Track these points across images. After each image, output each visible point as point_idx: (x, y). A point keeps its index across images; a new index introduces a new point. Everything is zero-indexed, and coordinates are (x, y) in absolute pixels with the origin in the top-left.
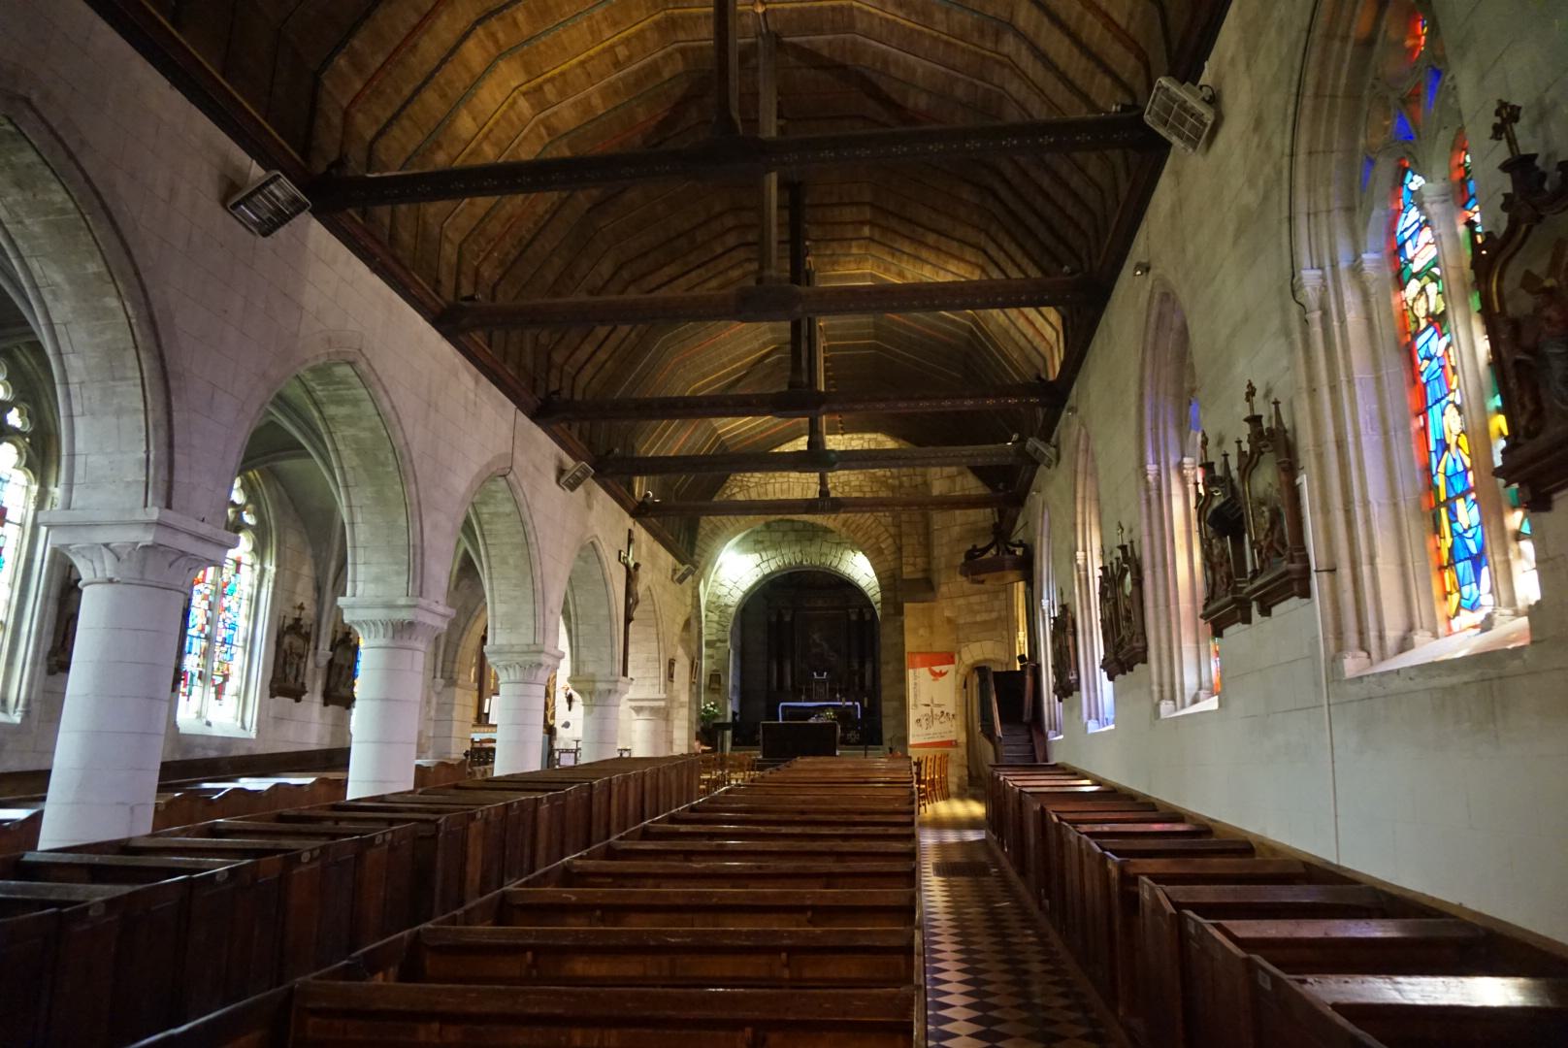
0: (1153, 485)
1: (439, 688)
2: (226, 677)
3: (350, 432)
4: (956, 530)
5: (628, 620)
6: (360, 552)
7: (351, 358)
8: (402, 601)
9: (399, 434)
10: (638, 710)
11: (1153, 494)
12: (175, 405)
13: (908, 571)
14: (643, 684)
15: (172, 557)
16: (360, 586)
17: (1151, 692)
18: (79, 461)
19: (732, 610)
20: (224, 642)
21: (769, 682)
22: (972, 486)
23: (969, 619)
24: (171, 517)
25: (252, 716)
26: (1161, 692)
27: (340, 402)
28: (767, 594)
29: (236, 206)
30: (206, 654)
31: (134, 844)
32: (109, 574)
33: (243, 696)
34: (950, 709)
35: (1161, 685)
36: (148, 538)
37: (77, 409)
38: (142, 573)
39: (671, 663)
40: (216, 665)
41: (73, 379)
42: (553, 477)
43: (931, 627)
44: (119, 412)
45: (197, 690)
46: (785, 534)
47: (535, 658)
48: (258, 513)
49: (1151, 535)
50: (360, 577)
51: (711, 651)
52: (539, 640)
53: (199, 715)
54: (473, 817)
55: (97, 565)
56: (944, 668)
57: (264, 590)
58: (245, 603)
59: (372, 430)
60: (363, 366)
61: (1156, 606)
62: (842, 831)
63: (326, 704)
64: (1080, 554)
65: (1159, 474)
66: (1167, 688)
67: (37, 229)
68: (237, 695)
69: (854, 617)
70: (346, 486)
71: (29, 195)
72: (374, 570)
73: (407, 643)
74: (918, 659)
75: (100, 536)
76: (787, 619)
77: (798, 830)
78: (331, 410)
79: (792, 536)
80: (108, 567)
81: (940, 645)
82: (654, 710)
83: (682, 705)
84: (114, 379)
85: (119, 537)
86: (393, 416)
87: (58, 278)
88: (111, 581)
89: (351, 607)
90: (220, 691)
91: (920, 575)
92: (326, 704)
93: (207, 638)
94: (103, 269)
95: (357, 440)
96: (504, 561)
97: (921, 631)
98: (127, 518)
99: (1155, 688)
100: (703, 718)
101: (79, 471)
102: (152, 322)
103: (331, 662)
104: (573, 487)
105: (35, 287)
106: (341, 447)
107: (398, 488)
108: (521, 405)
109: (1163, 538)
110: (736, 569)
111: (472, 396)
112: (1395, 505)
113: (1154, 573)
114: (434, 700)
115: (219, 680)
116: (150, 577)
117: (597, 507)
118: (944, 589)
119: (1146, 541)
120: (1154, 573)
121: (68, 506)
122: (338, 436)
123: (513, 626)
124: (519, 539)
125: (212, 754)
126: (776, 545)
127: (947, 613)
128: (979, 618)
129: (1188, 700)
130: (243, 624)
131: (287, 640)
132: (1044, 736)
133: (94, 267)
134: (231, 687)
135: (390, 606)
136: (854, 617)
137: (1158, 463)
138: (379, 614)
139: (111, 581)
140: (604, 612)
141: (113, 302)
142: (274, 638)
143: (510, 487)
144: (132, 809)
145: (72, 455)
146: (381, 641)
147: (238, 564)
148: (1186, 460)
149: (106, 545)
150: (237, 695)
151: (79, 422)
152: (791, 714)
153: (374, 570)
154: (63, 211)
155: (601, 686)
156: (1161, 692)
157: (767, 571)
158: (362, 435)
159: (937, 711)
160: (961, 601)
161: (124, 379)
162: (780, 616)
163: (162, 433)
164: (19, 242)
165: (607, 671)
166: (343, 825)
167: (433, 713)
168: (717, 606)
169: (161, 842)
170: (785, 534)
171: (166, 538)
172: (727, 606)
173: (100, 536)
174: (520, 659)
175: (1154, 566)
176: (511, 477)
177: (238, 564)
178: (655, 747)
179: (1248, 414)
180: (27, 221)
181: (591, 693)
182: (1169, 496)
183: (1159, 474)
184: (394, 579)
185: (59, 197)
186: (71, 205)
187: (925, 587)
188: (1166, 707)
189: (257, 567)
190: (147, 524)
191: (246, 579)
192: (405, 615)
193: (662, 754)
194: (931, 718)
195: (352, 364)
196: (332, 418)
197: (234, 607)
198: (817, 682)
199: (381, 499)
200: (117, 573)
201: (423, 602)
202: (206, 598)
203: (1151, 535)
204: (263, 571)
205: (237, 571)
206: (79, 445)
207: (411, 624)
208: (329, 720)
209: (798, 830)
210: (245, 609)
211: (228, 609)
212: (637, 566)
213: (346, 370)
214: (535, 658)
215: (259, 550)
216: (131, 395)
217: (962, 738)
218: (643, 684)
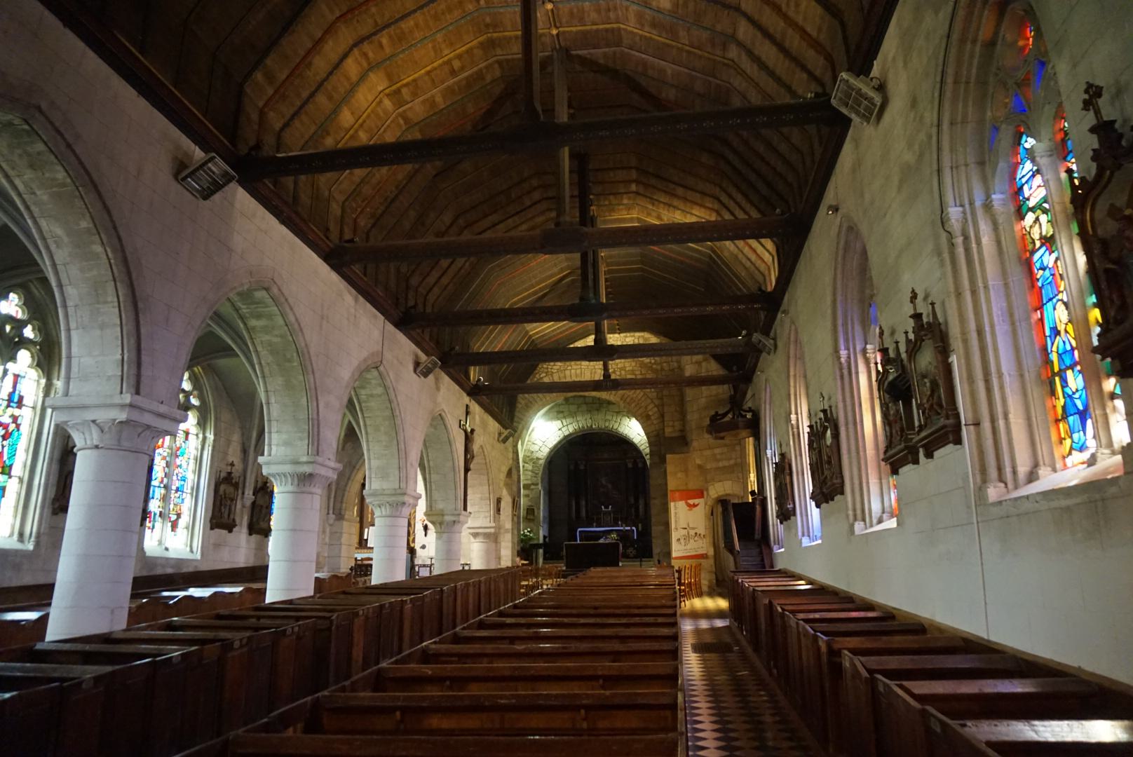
0: (845, 365)
1: (331, 521)
2: (179, 516)
3: (266, 338)
5: (467, 470)
6: (274, 424)
8: (304, 459)
9: (301, 339)
10: (475, 535)
11: (845, 372)
14: (478, 517)
15: (140, 430)
16: (274, 448)
17: (847, 516)
18: (75, 362)
19: (542, 462)
20: (177, 490)
22: (714, 368)
23: (714, 465)
24: (139, 400)
25: (198, 543)
26: (855, 516)
28: (567, 450)
29: (184, 179)
30: (165, 499)
31: (114, 636)
32: (95, 442)
33: (191, 528)
34: (702, 531)
35: (854, 510)
36: (123, 416)
37: (73, 325)
38: (119, 440)
39: (499, 501)
40: (172, 506)
41: (70, 303)
42: (411, 367)
43: (686, 471)
45: (158, 524)
47: (401, 499)
48: (201, 397)
50: (274, 442)
51: (527, 492)
52: (403, 485)
53: (160, 543)
54: (357, 614)
55: (88, 436)
56: (696, 501)
57: (205, 453)
58: (192, 462)
59: (282, 336)
60: (275, 290)
62: (624, 621)
64: (793, 417)
65: (849, 357)
66: (859, 512)
68: (187, 528)
69: (630, 465)
72: (284, 436)
73: (304, 489)
74: (677, 494)
75: (90, 415)
78: (253, 323)
79: (584, 407)
80: (95, 436)
81: (693, 484)
82: (487, 536)
83: (507, 531)
85: (103, 416)
87: (59, 231)
88: (97, 447)
89: (268, 463)
90: (174, 526)
93: (165, 487)
94: (91, 225)
95: (270, 344)
96: (377, 429)
97: (679, 475)
98: (109, 401)
99: (851, 513)
100: (522, 541)
101: (75, 369)
102: (125, 261)
103: (254, 503)
104: (426, 375)
106: (259, 349)
107: (301, 378)
109: (853, 405)
110: (544, 432)
111: (352, 311)
112: (1022, 376)
113: (847, 429)
114: (328, 530)
115: (174, 518)
116: (126, 444)
118: (695, 444)
121: (66, 394)
123: (384, 476)
124: (388, 413)
125: (170, 571)
126: (572, 415)
127: (698, 462)
128: (721, 464)
129: (875, 521)
130: (191, 477)
131: (222, 488)
133: (85, 224)
134: (183, 522)
135: (296, 463)
136: (630, 465)
138: (288, 468)
139: (97, 447)
140: (449, 464)
141: (98, 248)
142: (213, 487)
144: (112, 612)
145: (69, 357)
146: (290, 488)
147: (187, 434)
148: (868, 347)
149: (94, 421)
150: (187, 528)
151: (73, 333)
152: (586, 536)
153: (284, 436)
154: (64, 185)
155: (448, 518)
158: (276, 340)
159: (692, 532)
160: (708, 453)
161: (106, 302)
164: (33, 208)
167: (327, 540)
168: (530, 459)
171: (136, 416)
172: (538, 459)
173: (90, 415)
177: (187, 434)
178: (488, 561)
180: (38, 193)
181: (441, 524)
182: (857, 373)
183: (849, 357)
184: (299, 443)
185: (61, 175)
186: (69, 180)
187: (681, 442)
188: (859, 527)
189: (201, 436)
190: (123, 406)
191: (194, 443)
192: (307, 469)
193: (493, 567)
194: (687, 538)
195: (267, 289)
196: (254, 328)
197: (184, 465)
198: (605, 513)
199: (288, 386)
200: (102, 441)
201: (319, 459)
202: (164, 458)
204: (205, 439)
205: (187, 438)
206: (75, 350)
207: (311, 475)
208: (253, 545)
210: (192, 466)
211: (180, 466)
213: (264, 293)
214: (401, 499)
215: (202, 424)
216: (110, 313)
217: (711, 552)
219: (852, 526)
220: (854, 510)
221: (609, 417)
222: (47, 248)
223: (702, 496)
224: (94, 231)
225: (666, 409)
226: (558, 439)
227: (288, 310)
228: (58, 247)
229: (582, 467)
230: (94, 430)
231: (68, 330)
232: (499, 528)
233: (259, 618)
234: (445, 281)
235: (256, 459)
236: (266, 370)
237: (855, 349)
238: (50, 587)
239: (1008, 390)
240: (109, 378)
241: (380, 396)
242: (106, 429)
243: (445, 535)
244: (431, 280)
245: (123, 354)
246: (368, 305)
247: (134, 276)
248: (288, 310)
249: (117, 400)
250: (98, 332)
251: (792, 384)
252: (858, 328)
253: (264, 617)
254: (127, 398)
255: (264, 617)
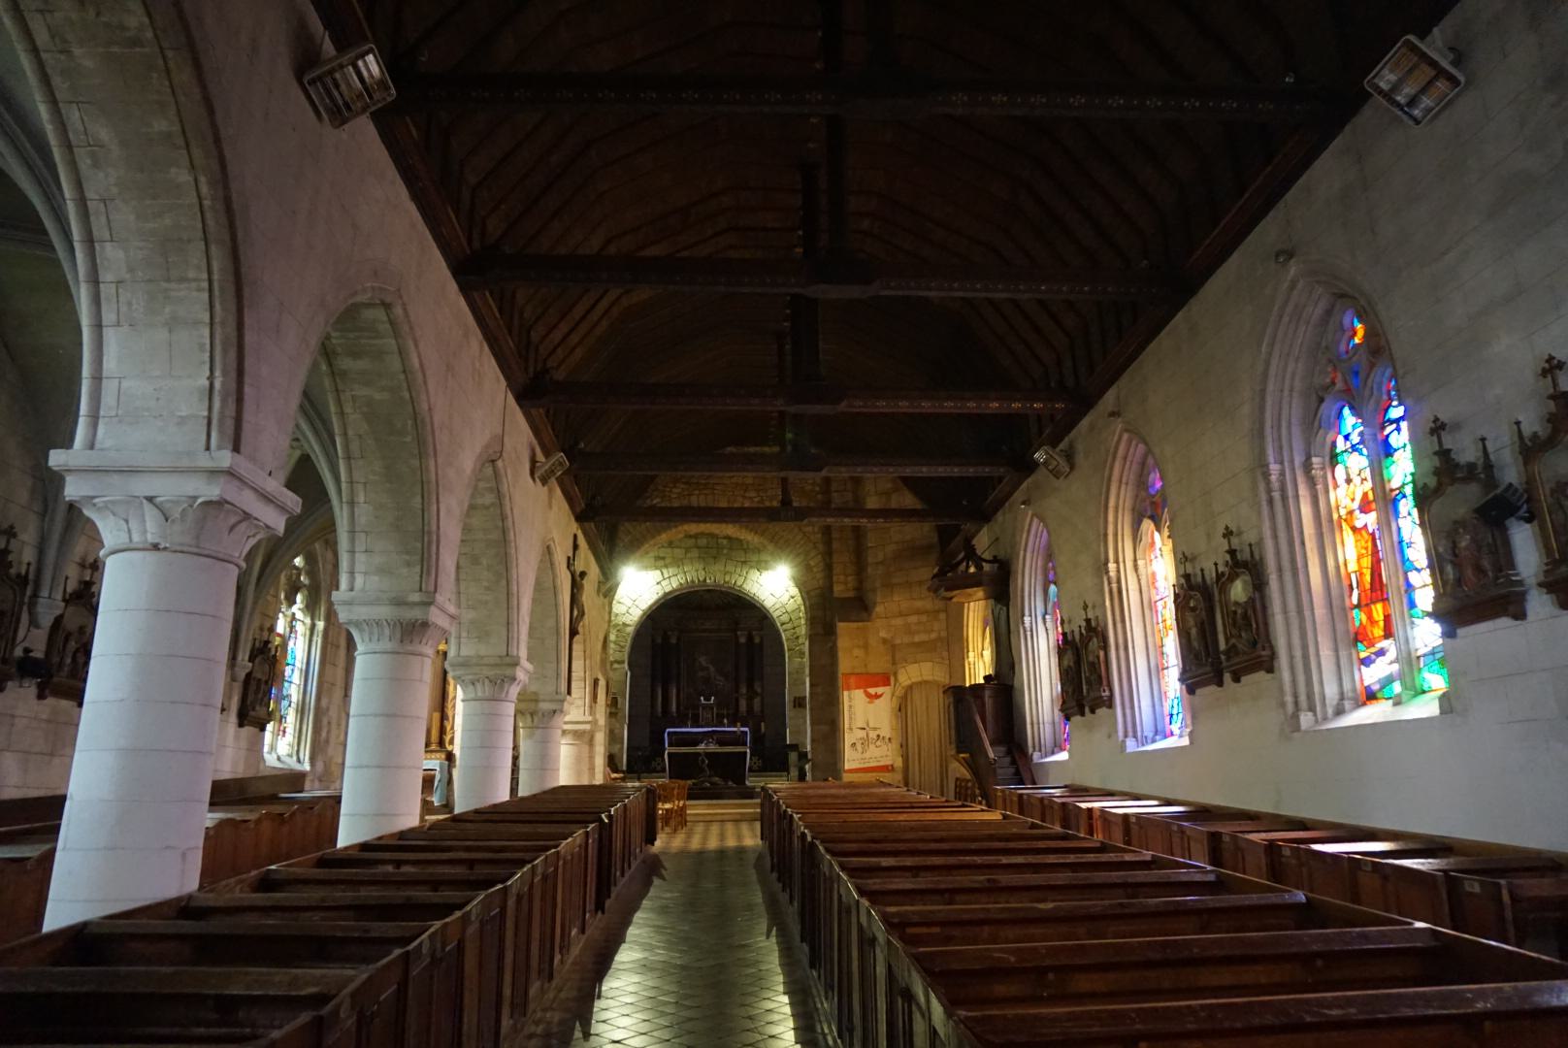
0: (1275, 485)
3: (362, 392)
4: (890, 548)
5: (573, 633)
6: (361, 538)
7: (388, 300)
9: (424, 397)
11: (1276, 495)
12: (247, 321)
13: (839, 590)
14: (577, 711)
15: (233, 520)
16: (359, 581)
17: (1283, 705)
18: (109, 389)
19: (630, 630)
21: (653, 706)
22: (908, 500)
23: (906, 640)
24: (244, 466)
26: (1296, 703)
27: (356, 355)
28: (665, 614)
32: (151, 538)
34: (886, 732)
35: (1296, 696)
36: (212, 491)
37: (108, 317)
38: (198, 537)
39: (596, 682)
41: (106, 276)
43: (866, 647)
44: (172, 323)
46: (687, 550)
47: (508, 672)
49: (1275, 537)
55: (134, 525)
56: (880, 690)
60: (398, 311)
61: (1285, 611)
63: (241, 725)
64: (1112, 566)
65: (1282, 474)
66: (1303, 698)
67: (89, 63)
69: (743, 640)
70: (348, 458)
71: (92, 13)
72: (378, 560)
73: (410, 648)
74: (852, 680)
75: (142, 486)
76: (674, 641)
77: (1019, 859)
79: (695, 553)
80: (151, 527)
81: (878, 664)
84: (168, 280)
85: (167, 488)
86: (420, 375)
87: (104, 134)
88: (156, 547)
89: (349, 603)
91: (851, 594)
92: (241, 725)
94: (176, 128)
97: (857, 652)
98: (185, 463)
99: (1289, 699)
101: (108, 399)
103: (249, 675)
105: (68, 146)
106: (348, 410)
107: (416, 463)
108: (510, 385)
109: (1291, 543)
110: (640, 586)
113: (1280, 577)
117: (555, 508)
118: (879, 609)
119: (1269, 544)
120: (1280, 577)
122: (346, 396)
124: (495, 535)
126: (677, 562)
127: (883, 634)
128: (917, 639)
129: (1330, 711)
132: (1028, 758)
136: (743, 640)
137: (1282, 463)
138: (384, 612)
139: (156, 547)
140: (551, 623)
141: (184, 177)
143: (496, 473)
144: (184, 855)
145: (98, 378)
146: (387, 645)
148: (1315, 460)
149: (150, 499)
151: (110, 335)
152: (680, 740)
155: (545, 706)
156: (1296, 703)
157: (668, 589)
158: (378, 396)
159: (873, 735)
160: (899, 622)
161: (182, 280)
162: (666, 638)
163: (233, 354)
164: (57, 81)
165: (551, 688)
166: (406, 869)
169: (210, 900)
170: (687, 550)
173: (142, 486)
174: (491, 673)
175: (1280, 569)
176: (500, 463)
178: (579, 773)
179: (1551, 391)
180: (77, 51)
182: (1297, 497)
183: (1282, 474)
184: (405, 571)
186: (149, 34)
187: (859, 606)
188: (1306, 719)
190: (213, 473)
192: (416, 614)
193: (586, 782)
194: (866, 742)
195: (387, 306)
196: (344, 374)
198: (705, 707)
203: (1275, 537)
206: (110, 364)
208: (244, 744)
209: (1019, 859)
212: (583, 574)
213: (380, 314)
214: (508, 672)
216: (193, 301)
217: (899, 763)
218: (577, 711)
219: (1295, 716)
220: (1296, 696)
221: (730, 568)
222: (73, 165)
223: (887, 683)
224: (180, 142)
225: (835, 558)
226: (655, 597)
227: (411, 343)
228: (96, 165)
229: (674, 641)
230: (150, 511)
231: (98, 326)
232: (594, 723)
233: (398, 864)
234: (575, 338)
235: (330, 595)
236: (355, 447)
237: (1292, 462)
238: (54, 805)
239: (1309, 554)
240: (182, 421)
241: (487, 508)
242: (176, 514)
243: (538, 732)
244: (557, 335)
245: (211, 378)
246: (1289, 196)
247: (240, 235)
248: (411, 343)
249: (204, 461)
250: (162, 335)
251: (1111, 518)
252: (1296, 431)
253: (407, 862)
254: (225, 458)
255: (407, 862)
